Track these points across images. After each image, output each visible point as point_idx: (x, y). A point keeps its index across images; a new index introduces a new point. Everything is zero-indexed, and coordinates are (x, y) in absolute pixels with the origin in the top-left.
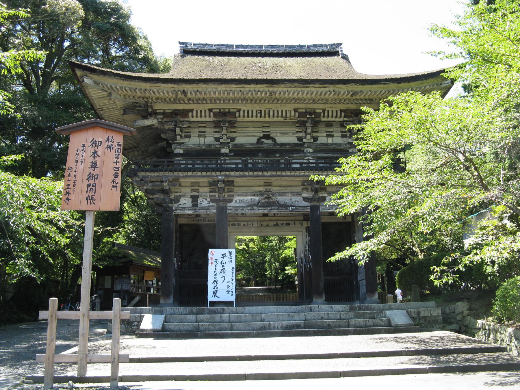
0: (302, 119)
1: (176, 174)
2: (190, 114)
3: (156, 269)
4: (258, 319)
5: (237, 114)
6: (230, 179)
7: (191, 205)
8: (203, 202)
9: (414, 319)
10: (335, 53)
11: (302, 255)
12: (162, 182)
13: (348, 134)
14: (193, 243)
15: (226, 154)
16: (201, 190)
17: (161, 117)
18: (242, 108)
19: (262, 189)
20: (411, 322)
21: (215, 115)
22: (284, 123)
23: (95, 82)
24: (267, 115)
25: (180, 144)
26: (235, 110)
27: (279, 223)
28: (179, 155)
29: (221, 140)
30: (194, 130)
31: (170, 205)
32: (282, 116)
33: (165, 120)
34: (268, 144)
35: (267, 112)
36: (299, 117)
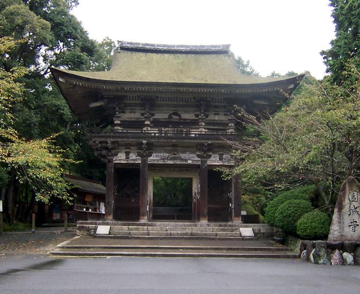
2: (126, 99)
17: (107, 100)
18: (159, 96)
20: (254, 235)
21: (142, 99)
26: (154, 97)
29: (145, 115)
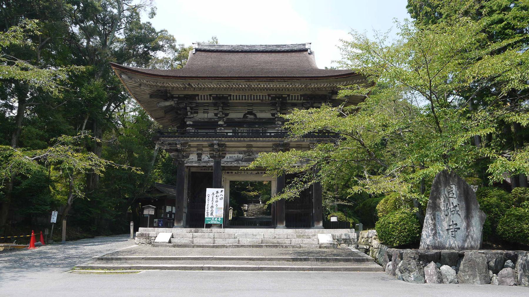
0: (274, 101)
2: (197, 98)
4: (233, 237)
5: (229, 98)
8: (205, 157)
15: (222, 125)
16: (204, 149)
18: (232, 94)
19: (245, 149)
21: (214, 98)
22: (262, 104)
23: (129, 78)
24: (250, 99)
25: (190, 118)
27: (260, 172)
28: (190, 125)
30: (201, 108)
31: (183, 160)
32: (260, 99)
33: (179, 101)
34: (251, 118)
35: (250, 96)
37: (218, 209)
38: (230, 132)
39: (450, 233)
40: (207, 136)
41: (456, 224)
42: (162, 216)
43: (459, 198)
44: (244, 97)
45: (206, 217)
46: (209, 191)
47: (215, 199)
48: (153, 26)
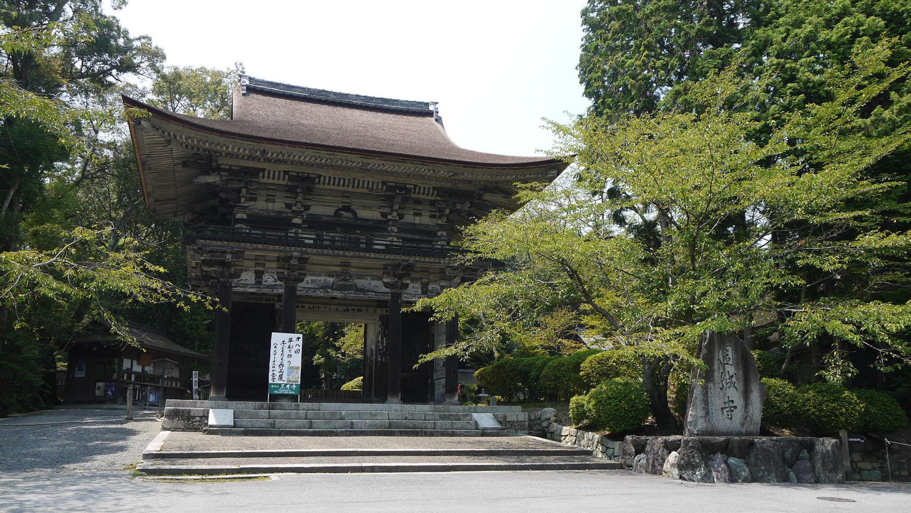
1: (243, 244)
2: (261, 174)
3: (209, 355)
4: (338, 417)
5: (317, 181)
6: (306, 256)
7: (254, 282)
8: (269, 279)
9: (500, 422)
10: (430, 114)
11: (373, 347)
12: (225, 252)
13: (438, 214)
14: (251, 326)
16: (268, 265)
19: (338, 269)
21: (291, 178)
23: (153, 126)
24: (351, 185)
27: (350, 308)
29: (294, 208)
31: (230, 280)
32: (367, 188)
35: (351, 181)
36: (386, 190)
37: (291, 369)
38: (309, 238)
39: (725, 413)
40: (278, 242)
41: (732, 401)
42: (115, 376)
43: (736, 365)
44: (342, 181)
45: (270, 381)
46: (277, 338)
47: (286, 352)
48: (123, 25)
